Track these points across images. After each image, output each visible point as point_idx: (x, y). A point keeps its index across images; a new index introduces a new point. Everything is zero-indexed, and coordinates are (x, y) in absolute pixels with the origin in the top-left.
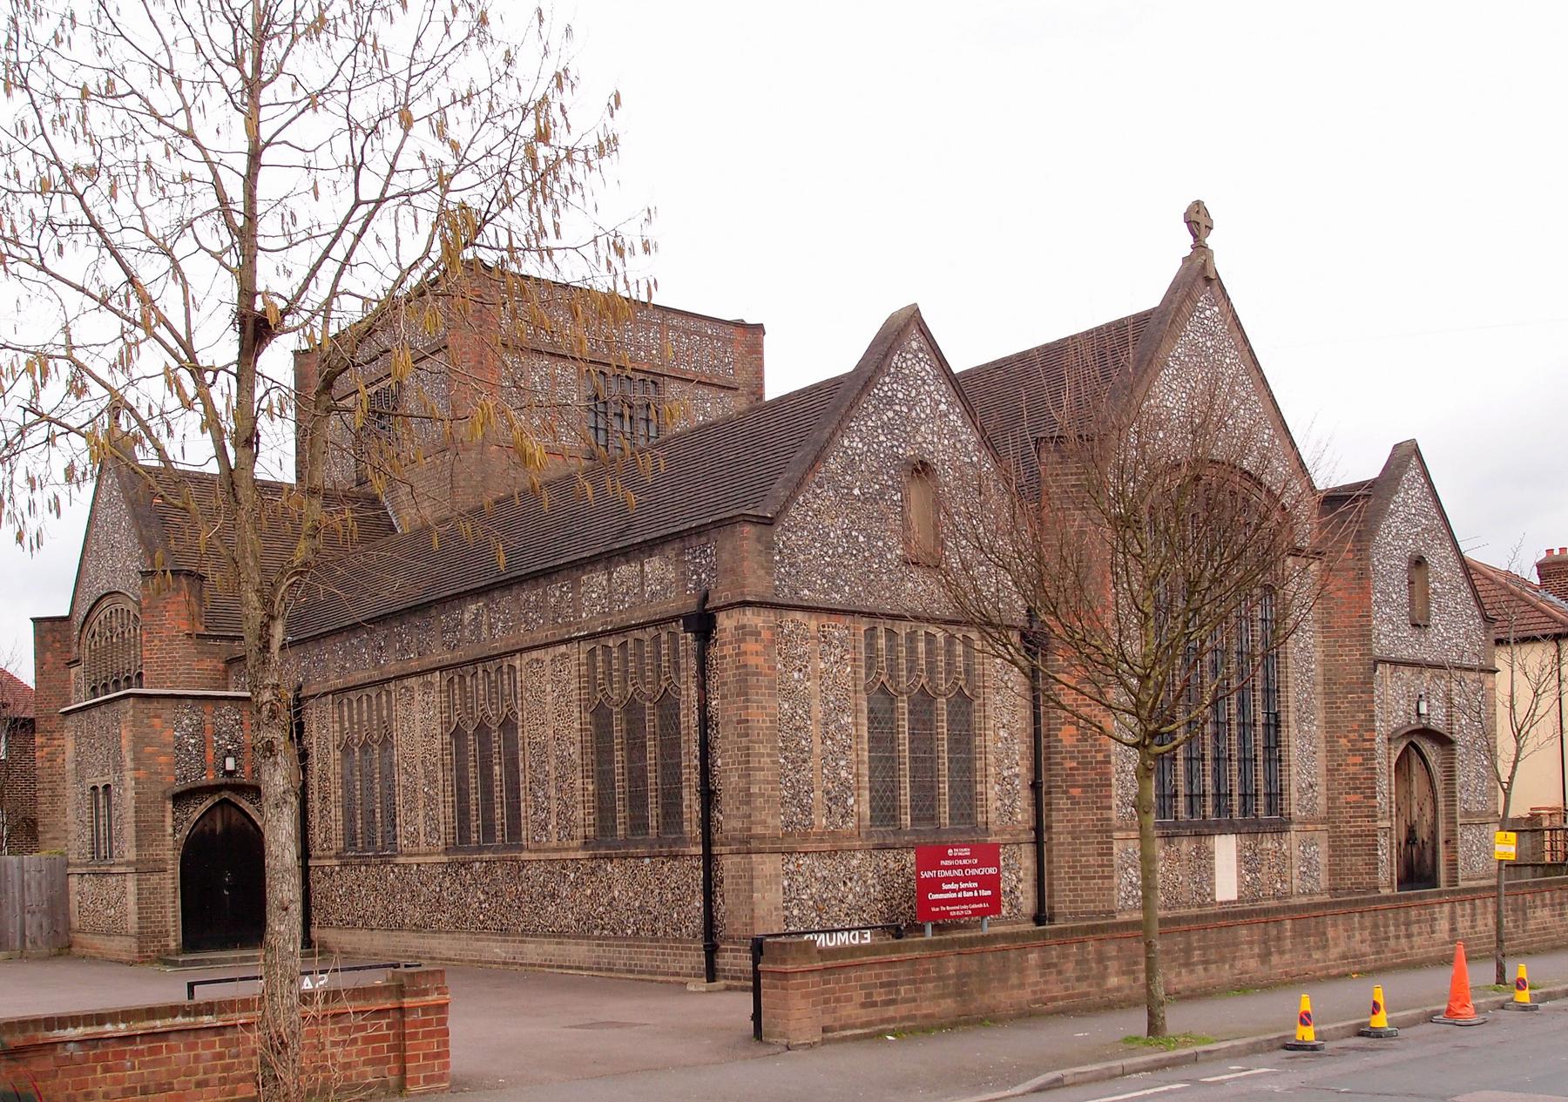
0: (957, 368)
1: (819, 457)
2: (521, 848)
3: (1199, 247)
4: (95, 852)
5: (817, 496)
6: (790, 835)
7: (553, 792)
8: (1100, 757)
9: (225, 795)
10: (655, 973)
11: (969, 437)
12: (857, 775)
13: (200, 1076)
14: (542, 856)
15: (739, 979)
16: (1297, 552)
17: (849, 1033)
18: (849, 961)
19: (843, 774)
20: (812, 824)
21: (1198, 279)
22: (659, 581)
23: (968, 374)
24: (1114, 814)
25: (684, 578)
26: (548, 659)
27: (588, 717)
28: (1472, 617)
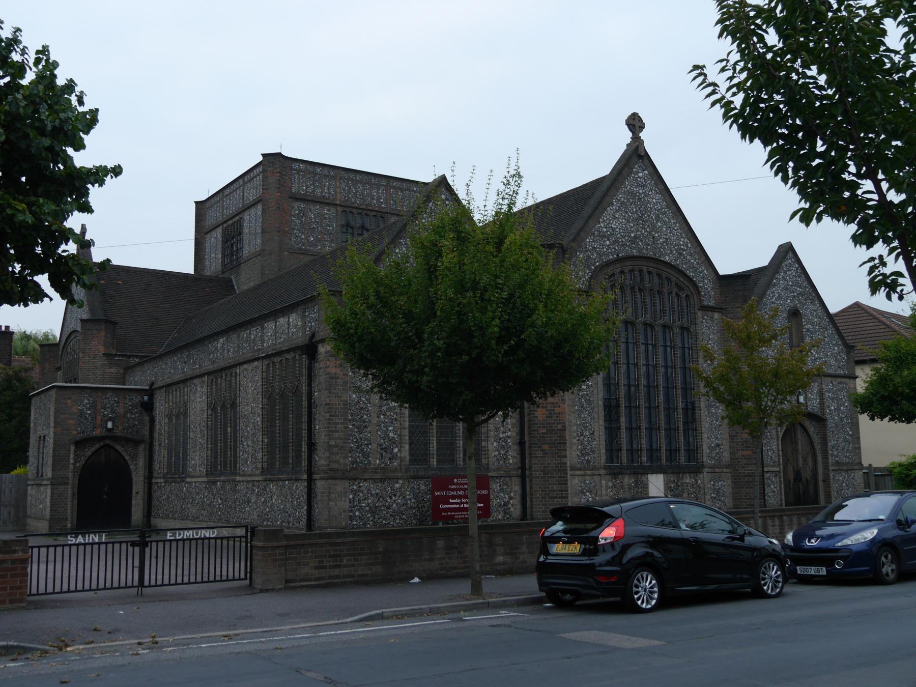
2: (235, 474)
6: (355, 469)
7: (250, 443)
8: (559, 427)
9: (107, 442)
10: (287, 547)
12: (400, 435)
16: (705, 309)
17: (306, 583)
18: (307, 542)
19: (391, 435)
20: (369, 463)
21: (636, 157)
25: (304, 325)
27: (265, 401)
28: (837, 345)
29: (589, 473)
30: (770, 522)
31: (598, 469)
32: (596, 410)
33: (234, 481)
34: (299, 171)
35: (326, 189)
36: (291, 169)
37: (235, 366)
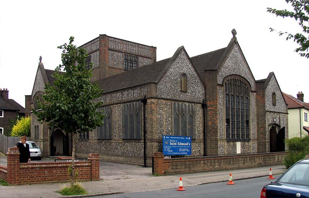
0: (190, 57)
1: (166, 72)
3: (234, 37)
4: (35, 137)
5: (165, 79)
7: (117, 130)
8: (216, 127)
11: (193, 69)
13: (58, 175)
14: (115, 141)
15: (150, 164)
16: (252, 91)
19: (169, 129)
21: (234, 42)
22: (136, 94)
23: (193, 58)
24: (218, 137)
26: (117, 106)
29: (222, 141)
30: (279, 156)
31: (224, 140)
32: (224, 122)
33: (110, 142)
34: (111, 41)
35: (120, 47)
36: (109, 40)
37: (110, 105)
